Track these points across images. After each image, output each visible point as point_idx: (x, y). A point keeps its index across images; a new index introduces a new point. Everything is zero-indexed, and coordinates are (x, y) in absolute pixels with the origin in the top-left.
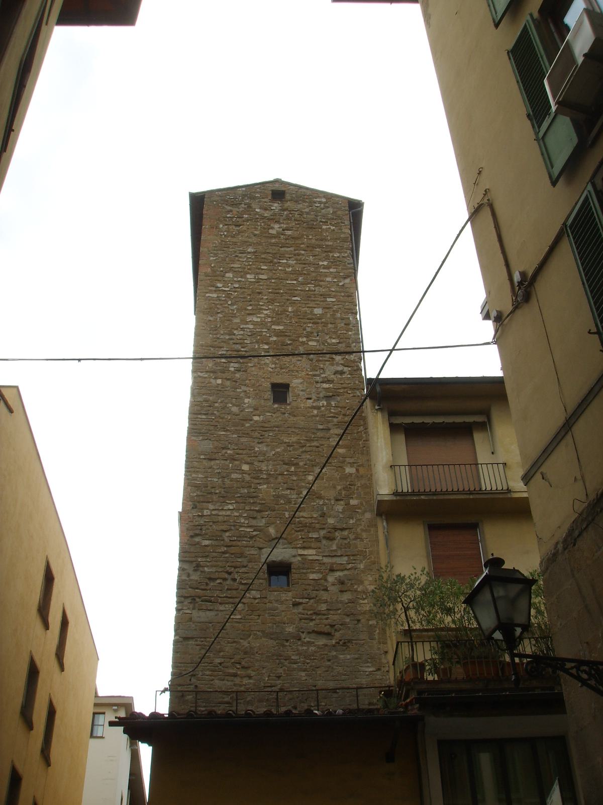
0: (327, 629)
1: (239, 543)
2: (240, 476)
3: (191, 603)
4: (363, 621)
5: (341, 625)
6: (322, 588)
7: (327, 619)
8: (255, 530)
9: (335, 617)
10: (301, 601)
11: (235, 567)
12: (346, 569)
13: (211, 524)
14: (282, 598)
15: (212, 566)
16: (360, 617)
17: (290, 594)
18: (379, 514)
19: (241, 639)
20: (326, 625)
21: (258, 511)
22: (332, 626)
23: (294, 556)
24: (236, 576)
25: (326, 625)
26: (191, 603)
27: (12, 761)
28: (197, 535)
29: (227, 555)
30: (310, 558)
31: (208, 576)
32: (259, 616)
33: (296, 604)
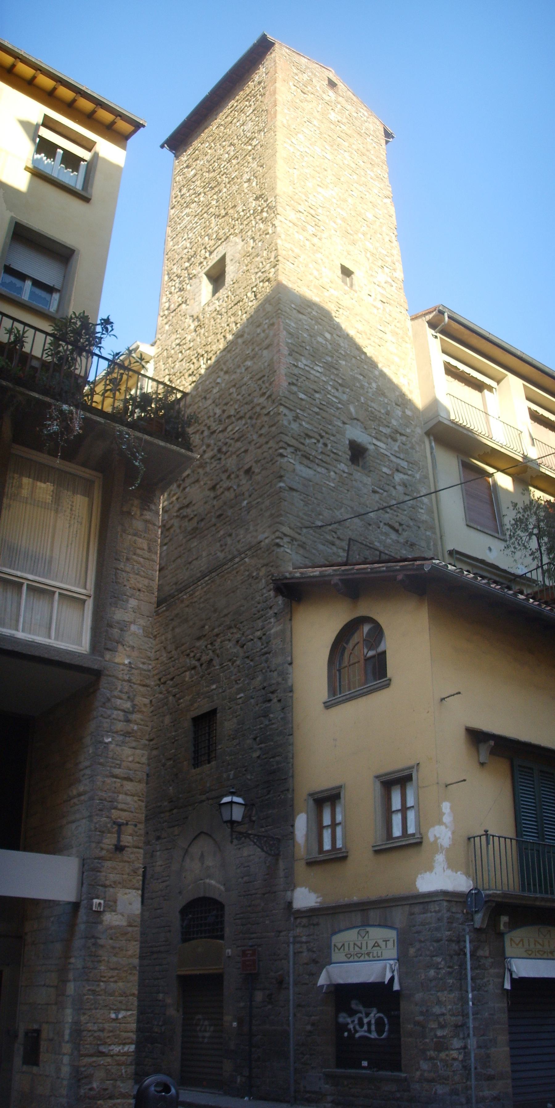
0: (396, 525)
1: (328, 409)
2: (324, 342)
3: (293, 453)
4: (422, 529)
5: (407, 526)
6: (393, 485)
7: (397, 516)
8: (339, 403)
9: (404, 517)
10: (378, 490)
11: (327, 433)
12: (407, 474)
13: (305, 378)
14: (364, 481)
15: (308, 423)
16: (421, 525)
17: (369, 479)
18: (428, 434)
19: (335, 508)
20: (397, 522)
21: (340, 385)
22: (401, 525)
23: (370, 443)
24: (328, 442)
25: (397, 522)
26: (293, 453)
27: (328, 705)
28: (293, 384)
29: (319, 417)
30: (382, 451)
31: (306, 432)
32: (348, 491)
33: (374, 492)
